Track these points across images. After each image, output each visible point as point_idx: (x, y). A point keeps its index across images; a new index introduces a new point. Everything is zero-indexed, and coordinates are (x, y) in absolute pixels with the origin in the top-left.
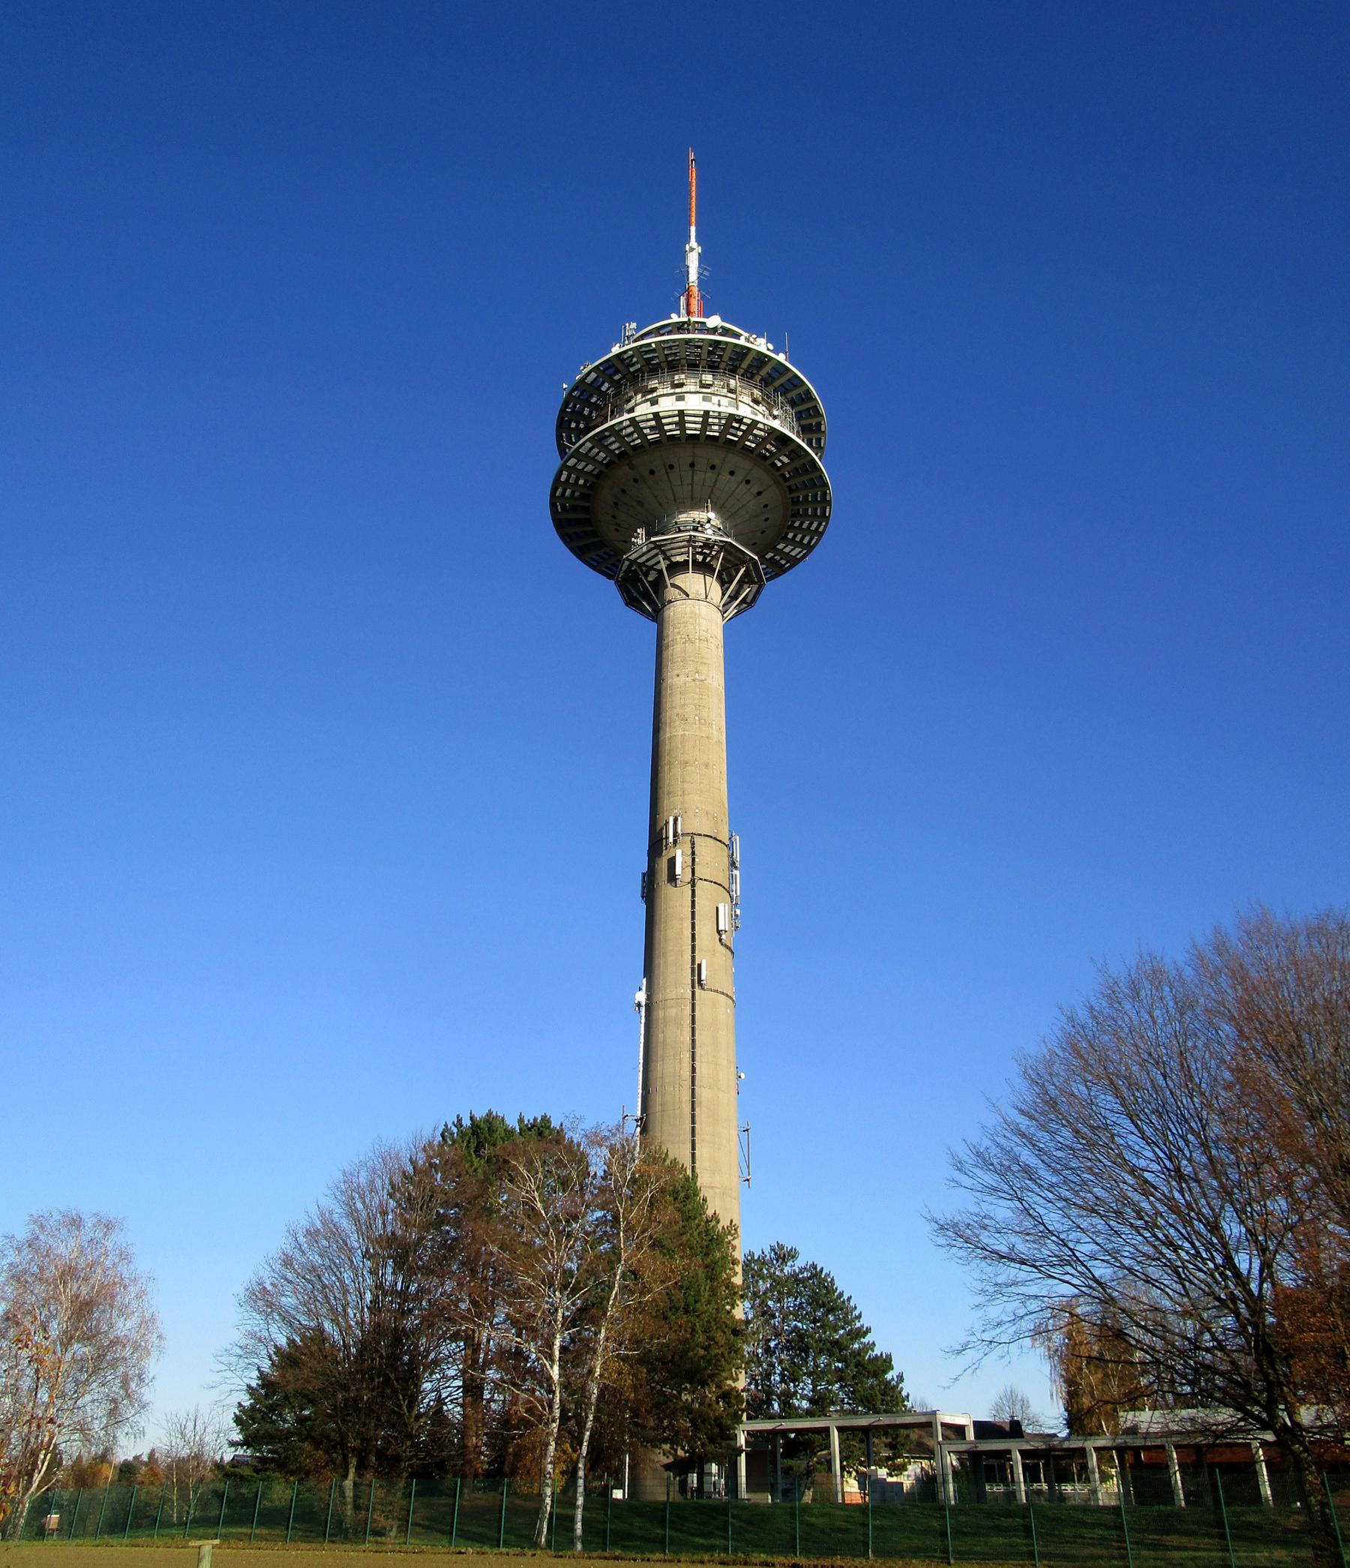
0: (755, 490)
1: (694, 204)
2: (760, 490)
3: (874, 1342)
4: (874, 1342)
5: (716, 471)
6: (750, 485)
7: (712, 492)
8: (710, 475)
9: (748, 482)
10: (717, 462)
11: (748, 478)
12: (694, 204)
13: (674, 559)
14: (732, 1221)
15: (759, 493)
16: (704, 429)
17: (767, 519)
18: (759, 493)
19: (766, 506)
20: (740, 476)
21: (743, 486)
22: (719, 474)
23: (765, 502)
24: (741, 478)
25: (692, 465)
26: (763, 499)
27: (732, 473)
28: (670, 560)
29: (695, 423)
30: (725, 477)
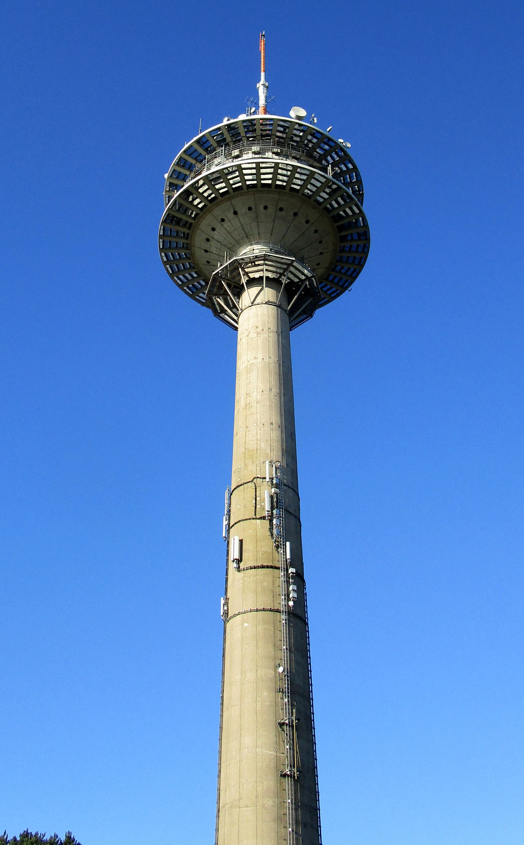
0: (231, 215)
1: (262, 60)
2: (232, 211)
3: (69, 832)
4: (69, 832)
5: (210, 239)
6: (226, 219)
7: (225, 246)
8: (213, 243)
9: (223, 220)
10: (205, 236)
11: (220, 220)
12: (262, 60)
13: (252, 276)
14: (269, 535)
15: (235, 213)
16: (274, 179)
17: (266, 208)
18: (235, 213)
19: (250, 209)
20: (218, 226)
21: (226, 224)
22: (213, 238)
23: (245, 209)
24: (220, 225)
25: (206, 251)
26: (242, 210)
27: (213, 229)
28: (249, 276)
29: (284, 175)
30: (215, 234)
